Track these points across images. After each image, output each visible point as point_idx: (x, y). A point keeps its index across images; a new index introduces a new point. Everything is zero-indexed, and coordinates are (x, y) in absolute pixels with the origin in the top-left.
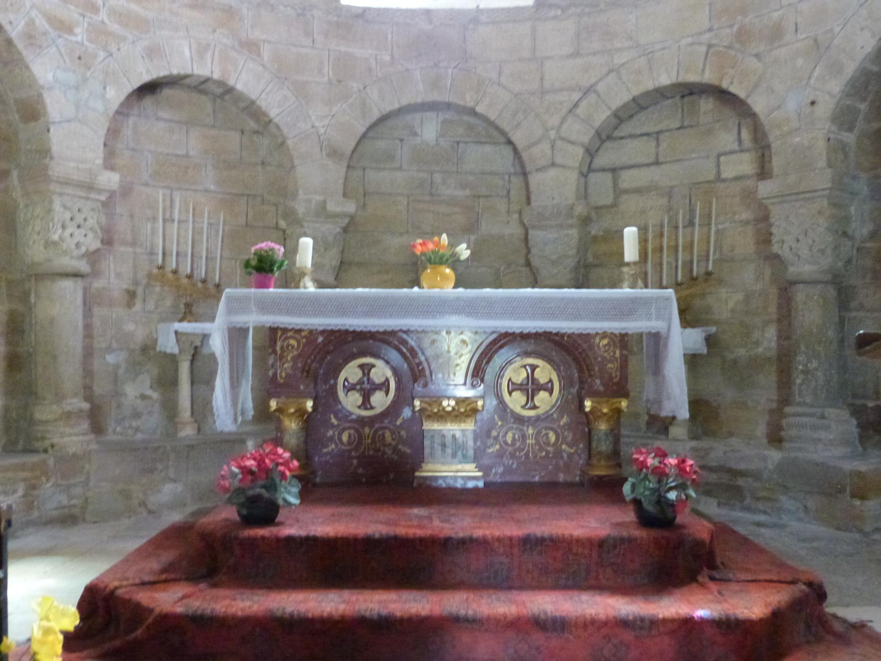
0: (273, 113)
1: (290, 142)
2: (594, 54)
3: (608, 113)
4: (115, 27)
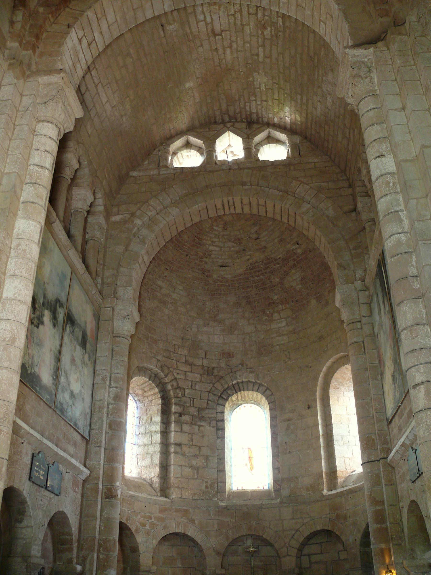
0: (199, 542)
1: (204, 551)
2: (298, 519)
3: (304, 538)
4: (156, 522)
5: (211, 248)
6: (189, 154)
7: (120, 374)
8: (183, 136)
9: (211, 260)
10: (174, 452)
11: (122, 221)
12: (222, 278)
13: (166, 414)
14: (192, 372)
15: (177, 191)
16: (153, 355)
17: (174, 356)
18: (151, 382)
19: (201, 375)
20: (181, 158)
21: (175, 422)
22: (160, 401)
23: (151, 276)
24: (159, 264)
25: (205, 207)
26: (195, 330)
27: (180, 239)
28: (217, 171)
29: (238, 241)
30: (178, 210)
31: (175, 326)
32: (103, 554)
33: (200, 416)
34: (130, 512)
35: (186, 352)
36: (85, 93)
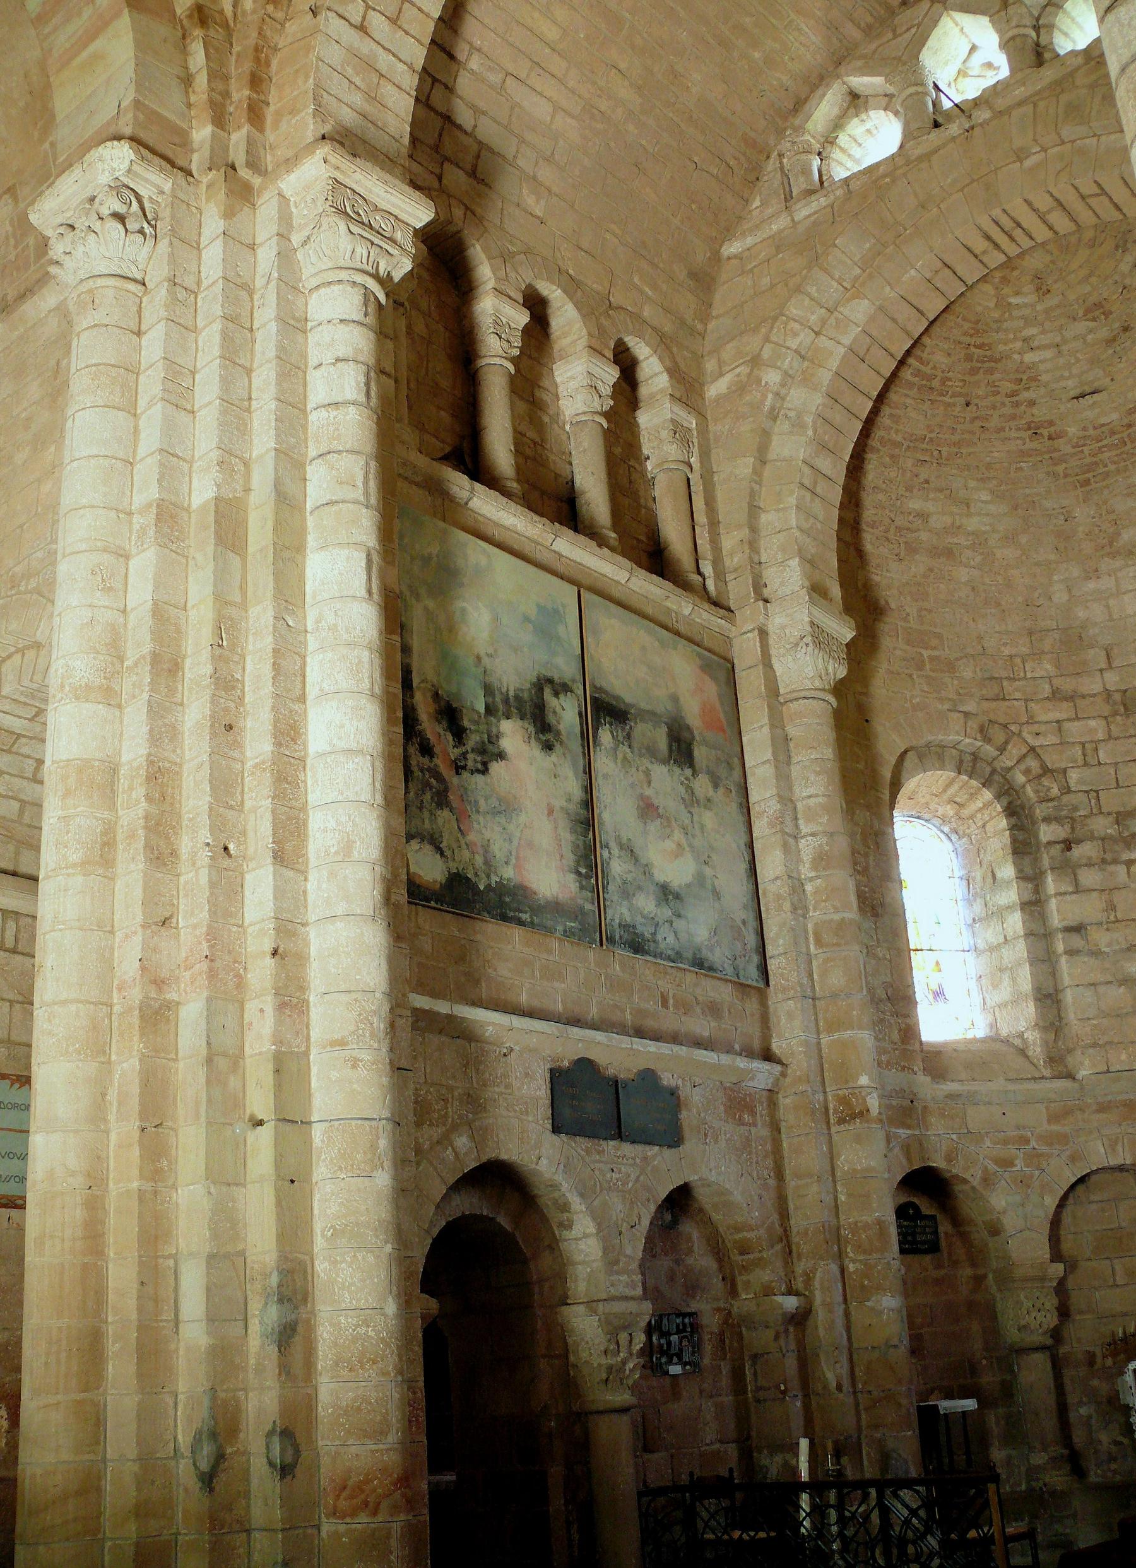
4: (1044, 1149)
5: (1029, 358)
6: (869, 125)
7: (817, 796)
8: (828, 86)
9: (1043, 390)
10: (1066, 953)
11: (734, 388)
12: (1095, 428)
13: (1030, 853)
14: (1078, 719)
15: (849, 250)
16: (946, 706)
17: (1016, 690)
18: (965, 778)
19: (1106, 718)
20: (854, 144)
21: (1052, 869)
22: (1003, 823)
23: (881, 496)
24: (892, 457)
25: (940, 264)
26: (1060, 596)
27: (927, 370)
28: (936, 151)
29: (1097, 310)
30: (866, 301)
31: (998, 604)
32: (854, 1261)
33: (1126, 834)
34: (954, 1137)
35: (1048, 667)
36: (475, 126)
